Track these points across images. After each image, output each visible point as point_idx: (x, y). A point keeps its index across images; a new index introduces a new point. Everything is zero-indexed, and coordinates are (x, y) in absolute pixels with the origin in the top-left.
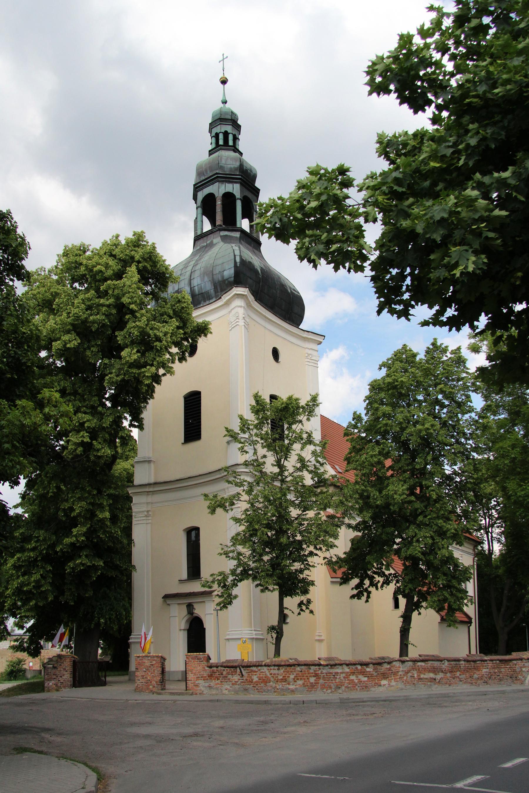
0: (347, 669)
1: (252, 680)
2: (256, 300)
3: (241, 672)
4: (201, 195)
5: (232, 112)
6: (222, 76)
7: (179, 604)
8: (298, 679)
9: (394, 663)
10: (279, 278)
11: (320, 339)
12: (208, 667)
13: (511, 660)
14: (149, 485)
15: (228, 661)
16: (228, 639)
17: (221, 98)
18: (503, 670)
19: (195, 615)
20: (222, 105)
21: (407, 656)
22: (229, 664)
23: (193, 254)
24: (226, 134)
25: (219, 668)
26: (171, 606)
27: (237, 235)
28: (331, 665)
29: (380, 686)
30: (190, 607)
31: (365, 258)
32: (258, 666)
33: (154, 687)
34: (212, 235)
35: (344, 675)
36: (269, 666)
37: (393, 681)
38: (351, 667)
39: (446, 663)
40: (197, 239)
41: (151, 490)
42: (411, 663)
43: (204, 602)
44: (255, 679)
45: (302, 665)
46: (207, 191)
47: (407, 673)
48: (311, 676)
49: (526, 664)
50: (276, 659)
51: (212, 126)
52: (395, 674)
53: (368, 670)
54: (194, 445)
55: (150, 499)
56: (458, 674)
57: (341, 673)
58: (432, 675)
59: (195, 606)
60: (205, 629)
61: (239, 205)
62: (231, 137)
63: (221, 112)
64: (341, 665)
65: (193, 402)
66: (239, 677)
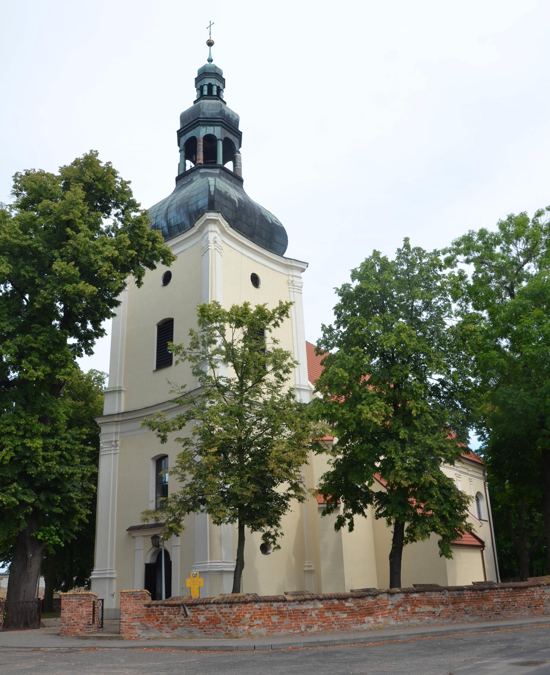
0: (320, 605)
1: (199, 620)
2: (231, 226)
3: (185, 611)
4: (184, 140)
5: (216, 67)
6: (209, 39)
7: (143, 536)
8: (255, 618)
9: (381, 596)
10: (259, 209)
12: (145, 605)
13: (526, 587)
18: (518, 599)
20: (208, 63)
21: (399, 586)
23: (174, 192)
24: (210, 86)
25: (159, 606)
27: (217, 171)
30: (155, 538)
32: (206, 604)
33: (81, 630)
34: (192, 174)
35: (317, 612)
37: (380, 617)
38: (325, 602)
39: (447, 593)
41: (120, 419)
42: (402, 596)
44: (202, 618)
45: (261, 602)
46: (189, 135)
47: (397, 607)
48: (272, 614)
49: (546, 591)
50: (235, 595)
51: (197, 80)
53: (347, 604)
54: (166, 372)
55: (119, 428)
56: (463, 605)
57: (312, 609)
58: (430, 608)
60: (171, 562)
64: (312, 599)
66: (183, 618)
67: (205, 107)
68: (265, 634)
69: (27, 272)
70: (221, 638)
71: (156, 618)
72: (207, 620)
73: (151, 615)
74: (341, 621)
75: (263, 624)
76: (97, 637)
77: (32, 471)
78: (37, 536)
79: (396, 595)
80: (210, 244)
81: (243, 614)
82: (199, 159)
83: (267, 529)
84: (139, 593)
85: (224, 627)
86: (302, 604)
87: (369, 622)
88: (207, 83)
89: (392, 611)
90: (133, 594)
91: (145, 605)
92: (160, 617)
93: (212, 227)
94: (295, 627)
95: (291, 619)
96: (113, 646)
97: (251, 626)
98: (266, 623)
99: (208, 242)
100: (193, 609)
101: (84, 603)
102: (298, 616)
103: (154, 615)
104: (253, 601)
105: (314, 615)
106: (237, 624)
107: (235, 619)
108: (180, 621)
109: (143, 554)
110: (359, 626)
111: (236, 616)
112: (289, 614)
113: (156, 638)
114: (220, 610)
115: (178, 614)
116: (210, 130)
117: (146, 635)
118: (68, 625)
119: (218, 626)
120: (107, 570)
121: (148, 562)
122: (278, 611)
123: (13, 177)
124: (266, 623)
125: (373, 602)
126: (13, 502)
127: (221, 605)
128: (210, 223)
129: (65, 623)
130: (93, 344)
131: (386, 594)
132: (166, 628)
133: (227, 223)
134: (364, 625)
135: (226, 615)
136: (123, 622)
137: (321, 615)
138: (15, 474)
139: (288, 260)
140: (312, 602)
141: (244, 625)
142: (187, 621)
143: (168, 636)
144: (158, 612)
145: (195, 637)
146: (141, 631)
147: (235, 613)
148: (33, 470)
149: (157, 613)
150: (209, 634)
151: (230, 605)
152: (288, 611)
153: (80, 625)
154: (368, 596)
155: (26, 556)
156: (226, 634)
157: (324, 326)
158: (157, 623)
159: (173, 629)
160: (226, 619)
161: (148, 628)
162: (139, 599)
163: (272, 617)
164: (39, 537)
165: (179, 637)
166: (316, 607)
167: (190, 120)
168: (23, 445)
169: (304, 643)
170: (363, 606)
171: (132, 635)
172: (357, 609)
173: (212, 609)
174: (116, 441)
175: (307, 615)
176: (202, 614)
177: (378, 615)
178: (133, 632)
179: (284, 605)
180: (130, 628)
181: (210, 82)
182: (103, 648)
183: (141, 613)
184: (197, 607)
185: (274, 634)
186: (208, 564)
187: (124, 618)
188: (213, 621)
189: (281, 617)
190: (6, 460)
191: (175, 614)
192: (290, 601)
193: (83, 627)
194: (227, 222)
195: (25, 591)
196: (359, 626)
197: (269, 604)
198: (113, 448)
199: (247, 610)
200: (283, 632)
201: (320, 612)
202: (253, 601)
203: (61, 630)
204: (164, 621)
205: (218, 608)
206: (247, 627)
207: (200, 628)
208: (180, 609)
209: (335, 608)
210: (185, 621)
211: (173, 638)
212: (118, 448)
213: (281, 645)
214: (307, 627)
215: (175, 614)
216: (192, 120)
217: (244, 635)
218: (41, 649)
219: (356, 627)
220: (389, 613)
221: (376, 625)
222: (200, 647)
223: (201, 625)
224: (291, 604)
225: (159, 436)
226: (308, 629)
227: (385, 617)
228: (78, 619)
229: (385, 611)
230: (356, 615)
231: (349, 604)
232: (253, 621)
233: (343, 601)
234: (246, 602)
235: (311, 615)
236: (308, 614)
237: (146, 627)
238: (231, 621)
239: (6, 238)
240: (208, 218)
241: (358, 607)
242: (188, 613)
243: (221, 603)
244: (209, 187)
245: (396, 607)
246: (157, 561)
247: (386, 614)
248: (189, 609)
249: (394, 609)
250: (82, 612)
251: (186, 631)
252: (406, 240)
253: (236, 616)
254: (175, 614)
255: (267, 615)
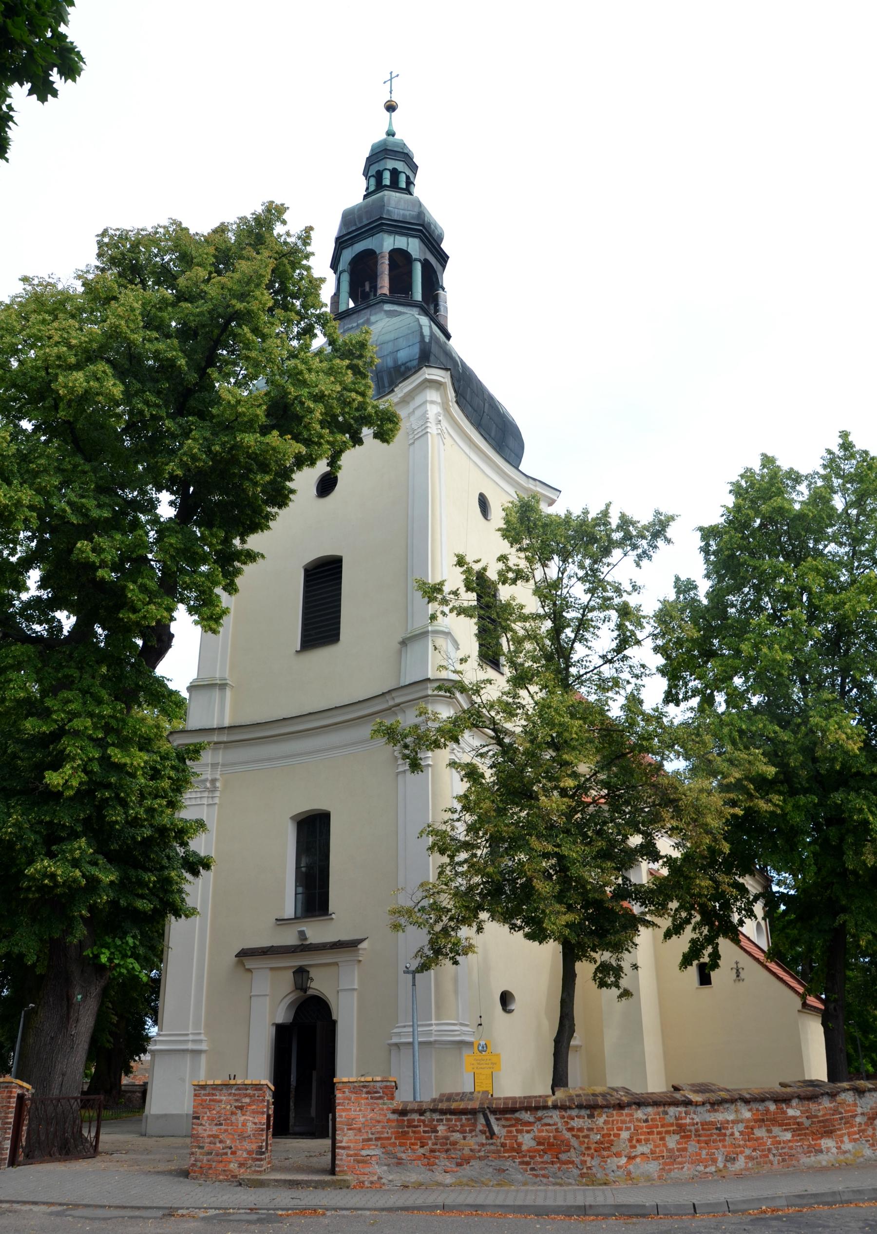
1: (520, 1145)
3: (488, 1124)
4: (348, 255)
7: (272, 969)
8: (639, 1141)
12: (394, 1112)
14: (221, 729)
15: (449, 1098)
16: (397, 1045)
19: (310, 992)
22: (454, 1106)
24: (395, 173)
25: (428, 1114)
26: (255, 972)
28: (713, 1104)
29: (821, 1151)
30: (301, 973)
32: (537, 1108)
33: (241, 1165)
35: (741, 1127)
36: (564, 1108)
37: (846, 1139)
38: (754, 1106)
41: (225, 739)
43: (336, 964)
44: (527, 1141)
46: (360, 247)
48: (668, 1132)
51: (371, 161)
52: (848, 1122)
53: (791, 1112)
54: (323, 655)
57: (733, 1122)
59: (313, 973)
61: (418, 269)
63: (384, 143)
64: (733, 1101)
65: (324, 579)
66: (482, 1139)
67: (393, 204)
68: (656, 1175)
69: (147, 403)
70: (570, 1184)
71: (420, 1139)
72: (539, 1144)
73: (408, 1133)
74: (783, 1148)
75: (653, 1152)
76: (285, 1181)
77: (116, 816)
78: (97, 956)
79: (867, 1094)
80: (429, 424)
81: (616, 1131)
82: (381, 287)
83: (605, 956)
84: (378, 1084)
85: (577, 1160)
86: (716, 1111)
87: (828, 1150)
88: (390, 167)
89: (863, 1127)
90: (364, 1087)
91: (394, 1112)
92: (430, 1138)
93: (432, 395)
94: (706, 1160)
95: (699, 1142)
96: (341, 1204)
97: (631, 1158)
98: (657, 1150)
99: (426, 420)
100: (507, 1119)
101: (249, 1105)
102: (711, 1135)
103: (414, 1132)
104: (635, 1103)
105: (737, 1134)
106: (605, 1153)
107: (602, 1143)
108: (477, 1147)
109: (269, 1004)
110: (813, 1159)
111: (603, 1136)
112: (697, 1130)
113: (419, 1185)
114: (567, 1123)
115: (471, 1131)
116: (401, 242)
117: (397, 1177)
118: (210, 1153)
119: (563, 1157)
120: (187, 1035)
121: (280, 1020)
122: (678, 1125)
123: (98, 236)
124: (657, 1150)
125: (830, 1109)
126: (75, 880)
127: (569, 1112)
128: (430, 387)
129: (202, 1148)
130: (238, 572)
131: (851, 1093)
132: (443, 1162)
133: (454, 395)
134: (820, 1157)
135: (581, 1134)
136: (343, 1148)
137: (748, 1134)
138: (77, 820)
139: (531, 481)
140: (733, 1107)
141: (618, 1155)
142: (493, 1147)
143: (448, 1179)
144: (425, 1126)
145: (511, 1183)
146: (385, 1168)
147: (600, 1129)
148: (118, 815)
149: (422, 1129)
150: (544, 1176)
151: (588, 1112)
152: (693, 1124)
153: (239, 1153)
154: (822, 1094)
155: (69, 999)
156: (582, 1175)
157: (677, 579)
158: (422, 1151)
159: (459, 1165)
160: (583, 1143)
161: (400, 1163)
162: (380, 1098)
163: (667, 1138)
164: (104, 959)
165: (473, 1182)
166: (741, 1117)
167: (361, 222)
168: (105, 760)
169: (787, 1197)
170: (816, 1116)
171: (365, 1178)
172: (807, 1123)
173: (551, 1122)
174: (214, 781)
175: (725, 1135)
176: (528, 1132)
177: (842, 1136)
178: (367, 1170)
179: (686, 1113)
180: (359, 1162)
182: (335, 1209)
183: (383, 1127)
184: (517, 1115)
185: (672, 1174)
186: (434, 1028)
187: (345, 1139)
188: (553, 1148)
189: (682, 1137)
190: (71, 787)
191: (463, 1132)
192: (697, 1104)
193: (246, 1159)
194: (455, 391)
195: (64, 1075)
196: (813, 1159)
197: (661, 1109)
198: (206, 794)
199: (623, 1122)
200: (688, 1170)
201: (746, 1127)
202: (635, 1103)
203: (193, 1165)
204: (438, 1147)
205: (563, 1117)
206: (624, 1160)
207: (521, 1163)
208: (476, 1120)
209: (770, 1120)
210: (488, 1147)
211: (460, 1184)
212: (217, 794)
213: (744, 1202)
214: (726, 1160)
215: (465, 1132)
216: (365, 222)
217: (619, 1177)
218: (180, 1212)
219: (808, 1160)
220: (859, 1131)
221: (842, 1157)
222: (570, 1207)
223: (525, 1156)
224: (699, 1109)
225: (405, 757)
226: (729, 1165)
227: (855, 1140)
228: (233, 1140)
229: (852, 1126)
230: (805, 1134)
231: (793, 1111)
232: (635, 1147)
233: (784, 1106)
234: (620, 1106)
235: (732, 1134)
236: (728, 1132)
237: (395, 1160)
238: (593, 1146)
239: (117, 327)
240: (428, 377)
241: (807, 1118)
242: (496, 1129)
243: (570, 1108)
244: (421, 328)
245: (869, 1119)
246: (294, 1020)
247: (855, 1133)
248: (497, 1119)
249: (866, 1124)
250: (244, 1125)
251: (491, 1170)
252: (844, 435)
253: (603, 1136)
254: (465, 1132)
255: (659, 1133)
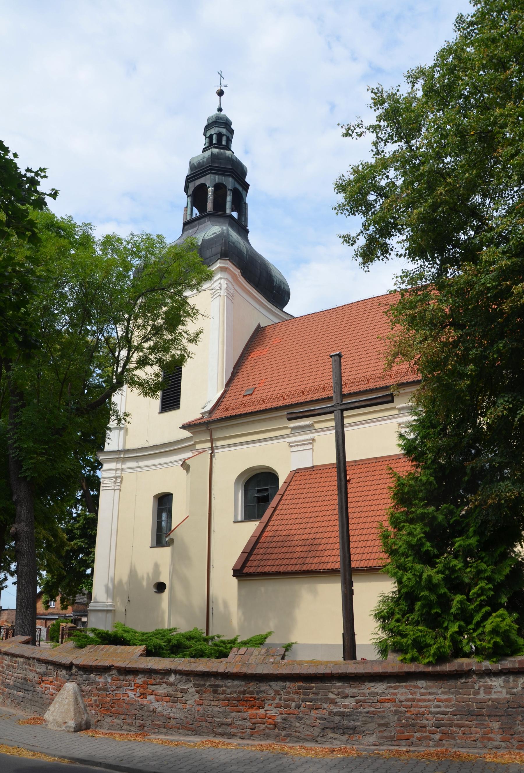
4: (192, 187)
11: (290, 416)
17: (217, 107)
31: (381, 236)
40: (185, 224)
62: (224, 139)
181: (220, 131)
